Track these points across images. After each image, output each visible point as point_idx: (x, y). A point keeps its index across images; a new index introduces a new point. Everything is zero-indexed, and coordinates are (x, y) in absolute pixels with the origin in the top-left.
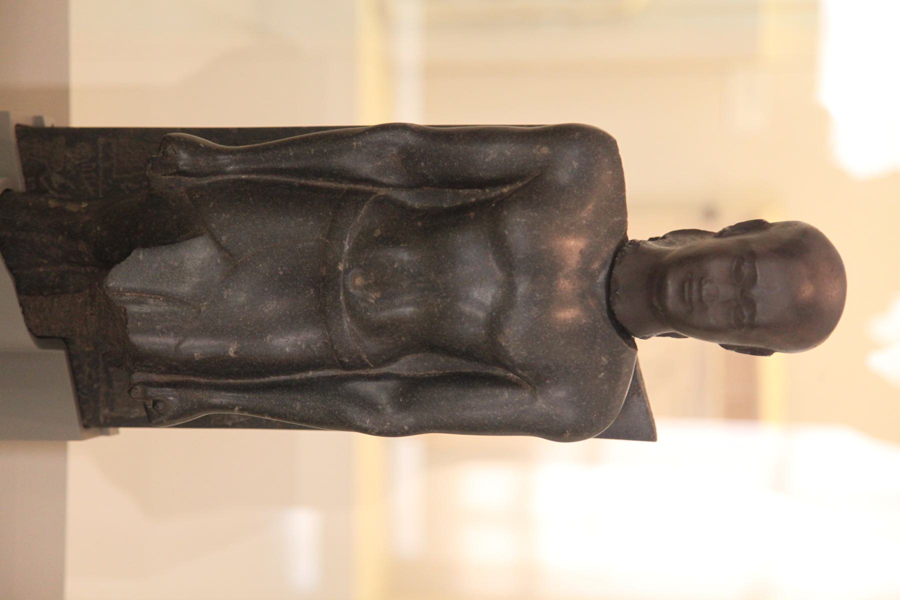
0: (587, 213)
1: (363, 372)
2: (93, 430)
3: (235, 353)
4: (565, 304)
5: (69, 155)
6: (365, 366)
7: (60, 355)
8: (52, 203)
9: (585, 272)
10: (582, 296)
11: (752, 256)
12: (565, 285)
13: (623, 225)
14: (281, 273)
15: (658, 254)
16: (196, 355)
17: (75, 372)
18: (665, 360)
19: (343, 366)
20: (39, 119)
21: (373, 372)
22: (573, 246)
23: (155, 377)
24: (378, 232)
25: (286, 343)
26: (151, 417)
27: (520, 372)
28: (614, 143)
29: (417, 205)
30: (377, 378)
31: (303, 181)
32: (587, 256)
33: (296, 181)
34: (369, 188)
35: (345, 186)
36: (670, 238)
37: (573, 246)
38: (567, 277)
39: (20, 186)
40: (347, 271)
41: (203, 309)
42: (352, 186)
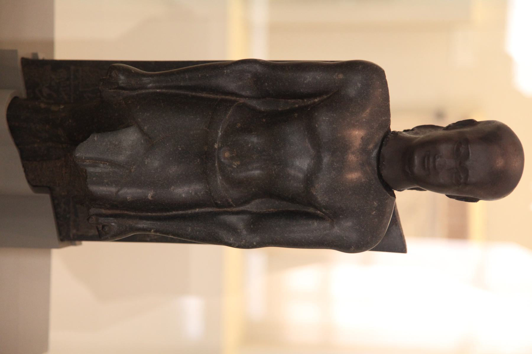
0: (366, 114)
1: (229, 210)
3: (152, 197)
6: (230, 206)
7: (46, 198)
8: (43, 106)
9: (364, 150)
11: (467, 142)
15: (409, 140)
17: (55, 207)
18: (412, 204)
19: (217, 206)
22: (357, 135)
23: (103, 211)
25: (183, 191)
27: (324, 210)
29: (262, 109)
31: (194, 94)
32: (365, 141)
33: (189, 93)
34: (234, 98)
35: (219, 97)
36: (416, 130)
37: (357, 135)
38: (353, 153)
40: (220, 148)
41: (133, 170)
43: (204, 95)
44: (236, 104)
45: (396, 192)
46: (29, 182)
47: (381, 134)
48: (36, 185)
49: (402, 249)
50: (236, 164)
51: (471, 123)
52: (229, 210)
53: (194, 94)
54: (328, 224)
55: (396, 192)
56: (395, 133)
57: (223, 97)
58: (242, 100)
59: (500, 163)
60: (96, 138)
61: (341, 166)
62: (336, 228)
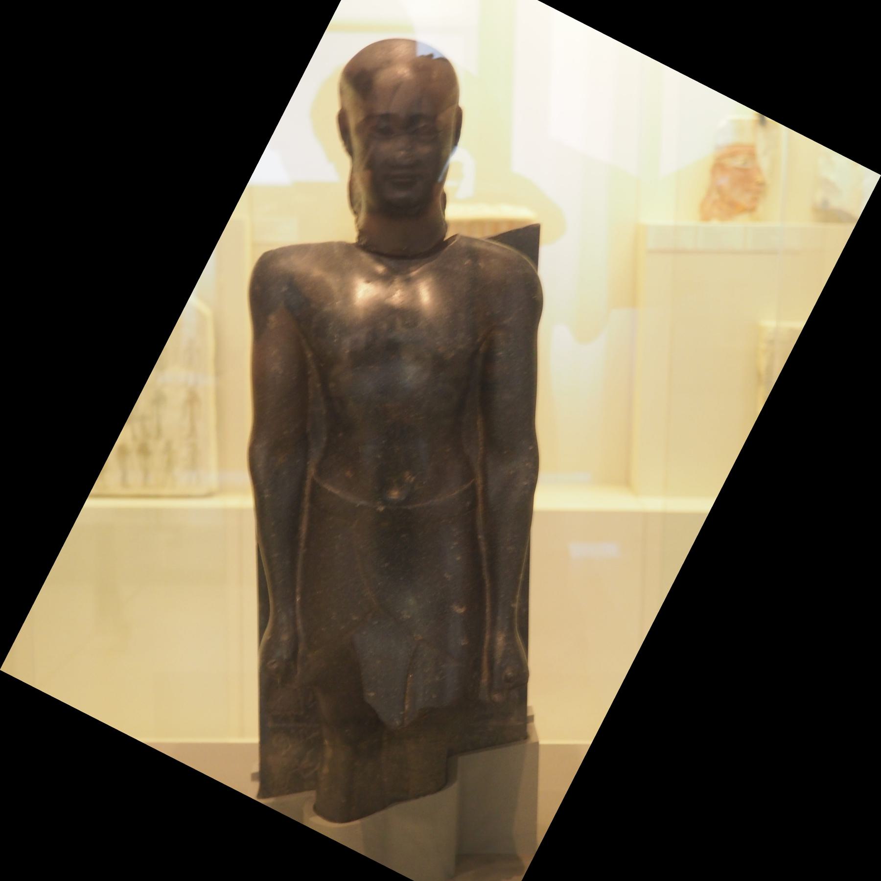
0: (332, 281)
1: (480, 489)
2: (529, 731)
3: (461, 607)
4: (415, 296)
5: (283, 753)
6: (473, 487)
7: (463, 761)
8: (326, 770)
9: (386, 279)
10: (408, 281)
11: (369, 117)
12: (397, 296)
13: (346, 248)
14: (386, 565)
15: (371, 211)
16: (463, 644)
17: (476, 747)
18: (472, 197)
19: (474, 506)
20: (254, 777)
21: (479, 481)
22: (365, 292)
23: (484, 681)
24: (348, 474)
25: (454, 559)
26: (517, 684)
27: (478, 340)
28: (266, 255)
29: (325, 439)
30: (485, 476)
31: (302, 544)
32: (373, 277)
33: (302, 552)
34: (308, 483)
35: (306, 505)
36: (356, 208)
37: (365, 292)
38: (390, 296)
39: (312, 794)
40: (385, 502)
41: (420, 637)
42: (306, 499)
43: (304, 529)
44: (525, 258)
45: (449, 235)
46: (440, 789)
47: (365, 257)
48: (442, 779)
49: (525, 240)
50: (409, 478)
51: (342, 119)
52: (480, 489)
53: (302, 544)
54: (500, 335)
55: (449, 235)
56: (362, 233)
57: (306, 499)
58: (312, 471)
59: (403, 71)
60: (372, 694)
61: (407, 315)
62: (505, 322)
